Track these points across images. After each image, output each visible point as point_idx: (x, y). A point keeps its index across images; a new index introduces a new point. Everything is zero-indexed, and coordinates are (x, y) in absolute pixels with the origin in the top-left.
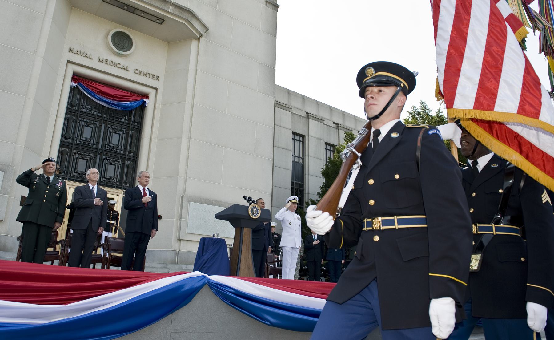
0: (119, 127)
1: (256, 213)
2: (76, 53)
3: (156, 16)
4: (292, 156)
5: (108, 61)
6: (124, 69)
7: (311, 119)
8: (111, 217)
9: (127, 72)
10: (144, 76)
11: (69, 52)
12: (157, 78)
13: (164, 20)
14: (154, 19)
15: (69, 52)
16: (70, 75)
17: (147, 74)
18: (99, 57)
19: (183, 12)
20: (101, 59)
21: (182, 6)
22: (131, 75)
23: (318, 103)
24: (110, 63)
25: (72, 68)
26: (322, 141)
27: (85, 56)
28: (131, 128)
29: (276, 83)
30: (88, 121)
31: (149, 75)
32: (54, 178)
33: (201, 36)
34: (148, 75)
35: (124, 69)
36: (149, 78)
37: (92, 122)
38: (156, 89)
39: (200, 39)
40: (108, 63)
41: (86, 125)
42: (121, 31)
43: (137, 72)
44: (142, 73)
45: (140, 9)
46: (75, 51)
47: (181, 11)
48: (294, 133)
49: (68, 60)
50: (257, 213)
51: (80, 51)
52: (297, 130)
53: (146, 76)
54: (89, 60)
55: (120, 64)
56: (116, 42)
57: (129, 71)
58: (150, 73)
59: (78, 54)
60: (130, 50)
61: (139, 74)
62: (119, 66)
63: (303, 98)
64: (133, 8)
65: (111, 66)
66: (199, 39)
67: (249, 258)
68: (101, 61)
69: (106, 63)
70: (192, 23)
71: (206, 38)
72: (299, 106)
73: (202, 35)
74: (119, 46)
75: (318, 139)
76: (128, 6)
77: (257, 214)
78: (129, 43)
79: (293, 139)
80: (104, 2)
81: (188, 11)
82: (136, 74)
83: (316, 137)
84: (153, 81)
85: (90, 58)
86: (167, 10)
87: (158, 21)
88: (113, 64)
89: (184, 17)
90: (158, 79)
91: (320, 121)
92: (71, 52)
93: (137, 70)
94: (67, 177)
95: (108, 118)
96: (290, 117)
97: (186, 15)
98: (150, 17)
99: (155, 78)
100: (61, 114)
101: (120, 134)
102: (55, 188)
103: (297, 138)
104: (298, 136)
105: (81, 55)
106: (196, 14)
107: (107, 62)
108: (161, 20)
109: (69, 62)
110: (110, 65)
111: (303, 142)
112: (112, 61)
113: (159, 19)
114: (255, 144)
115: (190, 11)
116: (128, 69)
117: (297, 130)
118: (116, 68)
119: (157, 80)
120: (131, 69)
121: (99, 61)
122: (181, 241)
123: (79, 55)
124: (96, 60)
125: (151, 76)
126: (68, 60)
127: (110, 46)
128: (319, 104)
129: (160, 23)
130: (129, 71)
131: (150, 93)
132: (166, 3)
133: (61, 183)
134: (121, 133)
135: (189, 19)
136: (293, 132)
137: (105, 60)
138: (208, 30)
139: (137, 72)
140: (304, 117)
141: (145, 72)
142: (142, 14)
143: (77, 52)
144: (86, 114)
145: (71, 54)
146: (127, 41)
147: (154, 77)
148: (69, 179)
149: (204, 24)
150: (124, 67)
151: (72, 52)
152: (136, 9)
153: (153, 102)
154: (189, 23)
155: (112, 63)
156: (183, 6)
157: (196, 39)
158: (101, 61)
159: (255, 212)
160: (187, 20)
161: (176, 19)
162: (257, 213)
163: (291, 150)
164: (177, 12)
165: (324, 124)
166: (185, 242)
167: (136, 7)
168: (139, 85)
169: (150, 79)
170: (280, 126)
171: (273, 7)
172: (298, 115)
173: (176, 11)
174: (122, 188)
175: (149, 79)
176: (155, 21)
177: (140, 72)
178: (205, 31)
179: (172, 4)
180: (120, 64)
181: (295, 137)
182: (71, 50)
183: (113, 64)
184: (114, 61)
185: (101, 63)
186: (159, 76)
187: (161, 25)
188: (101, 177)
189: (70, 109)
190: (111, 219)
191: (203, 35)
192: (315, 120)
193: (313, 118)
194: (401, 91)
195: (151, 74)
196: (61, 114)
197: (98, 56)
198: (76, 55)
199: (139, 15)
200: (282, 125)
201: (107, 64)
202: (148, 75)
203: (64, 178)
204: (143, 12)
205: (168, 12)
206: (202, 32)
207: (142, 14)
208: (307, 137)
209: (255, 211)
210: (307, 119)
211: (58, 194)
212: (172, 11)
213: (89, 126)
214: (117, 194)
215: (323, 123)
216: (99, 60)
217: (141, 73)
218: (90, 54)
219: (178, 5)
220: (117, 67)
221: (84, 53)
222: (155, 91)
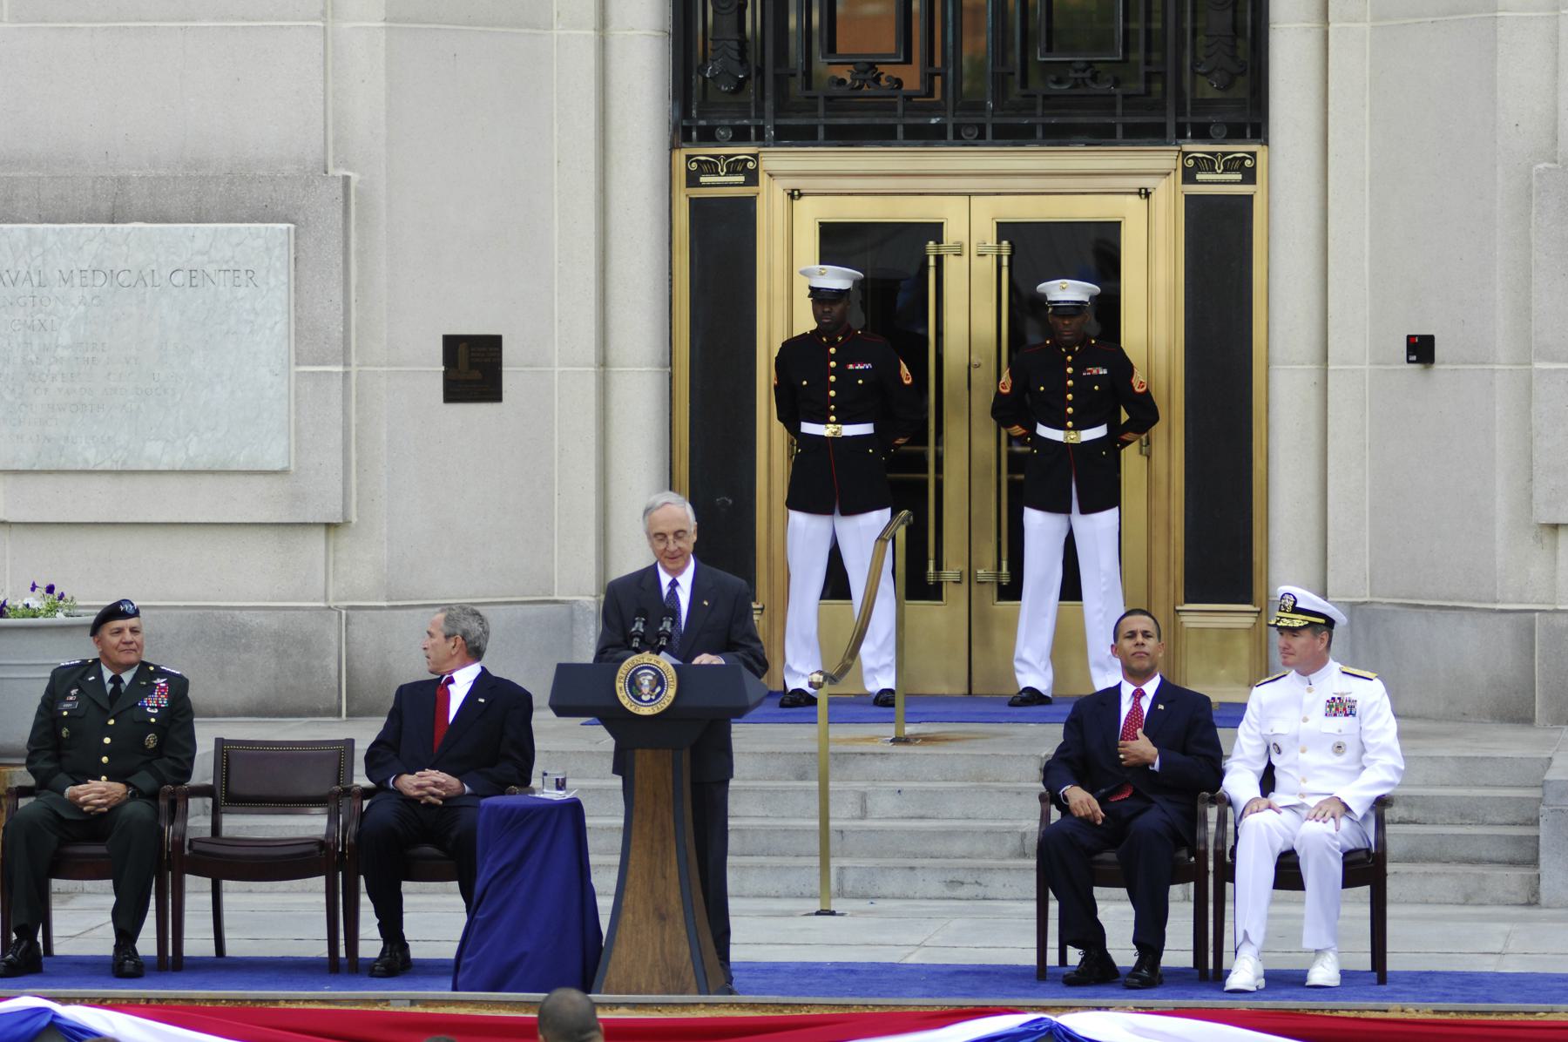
1: (653, 691)
8: (1070, 404)
32: (135, 678)
50: (658, 689)
67: (664, 877)
77: (658, 695)
102: (135, 722)
133: (161, 688)
148: (776, 128)
159: (646, 690)
162: (658, 689)
188: (932, 76)
190: (1070, 417)
203: (748, 128)
209: (646, 683)
211: (151, 740)
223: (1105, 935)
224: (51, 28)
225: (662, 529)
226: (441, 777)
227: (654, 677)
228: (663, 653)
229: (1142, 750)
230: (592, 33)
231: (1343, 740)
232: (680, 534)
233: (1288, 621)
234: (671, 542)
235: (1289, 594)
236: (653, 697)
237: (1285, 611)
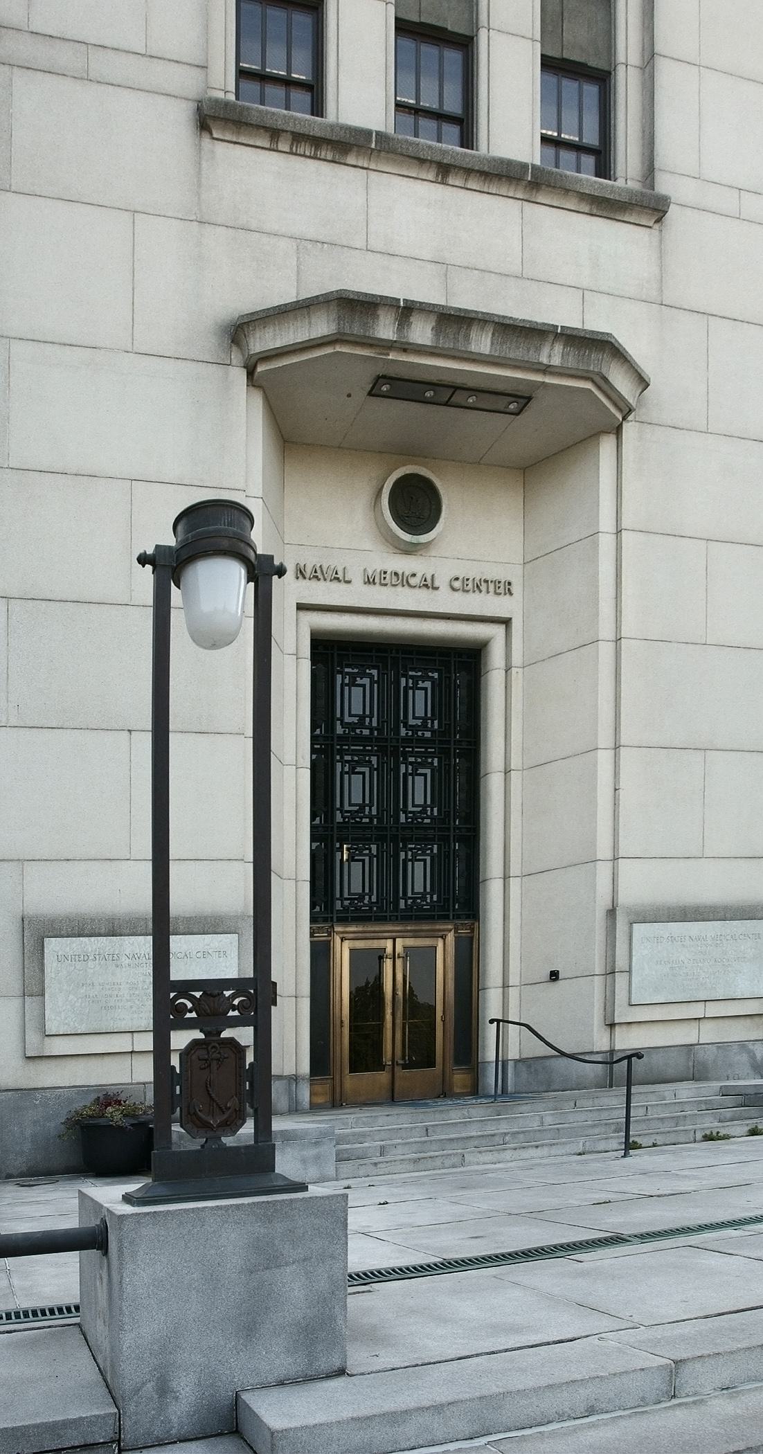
2: (424, 585)
6: (338, 579)
9: (436, 592)
11: (296, 580)
17: (482, 583)
18: (365, 570)
38: (507, 622)
40: (388, 580)
42: (408, 472)
43: (457, 584)
45: (471, 384)
49: (297, 603)
51: (321, 566)
54: (343, 586)
55: (414, 575)
57: (437, 588)
58: (489, 578)
60: (438, 525)
65: (393, 589)
69: (383, 582)
85: (346, 579)
88: (402, 580)
90: (509, 589)
93: (457, 579)
94: (332, 913)
98: (488, 402)
101: (363, 774)
109: (301, 607)
112: (396, 574)
116: (437, 584)
121: (365, 583)
122: (617, 1028)
123: (319, 580)
124: (358, 580)
126: (297, 603)
132: (629, 369)
134: (366, 770)
137: (381, 574)
138: (649, 385)
139: (457, 584)
151: (305, 578)
161: (567, 384)
166: (624, 1028)
169: (491, 597)
174: (451, 917)
176: (502, 409)
177: (383, 576)
183: (402, 580)
194: (598, 148)
196: (303, 758)
197: (362, 569)
198: (314, 583)
199: (462, 407)
204: (513, 399)
213: (418, 772)
214: (440, 934)
216: (366, 580)
218: (344, 568)
222: (498, 631)
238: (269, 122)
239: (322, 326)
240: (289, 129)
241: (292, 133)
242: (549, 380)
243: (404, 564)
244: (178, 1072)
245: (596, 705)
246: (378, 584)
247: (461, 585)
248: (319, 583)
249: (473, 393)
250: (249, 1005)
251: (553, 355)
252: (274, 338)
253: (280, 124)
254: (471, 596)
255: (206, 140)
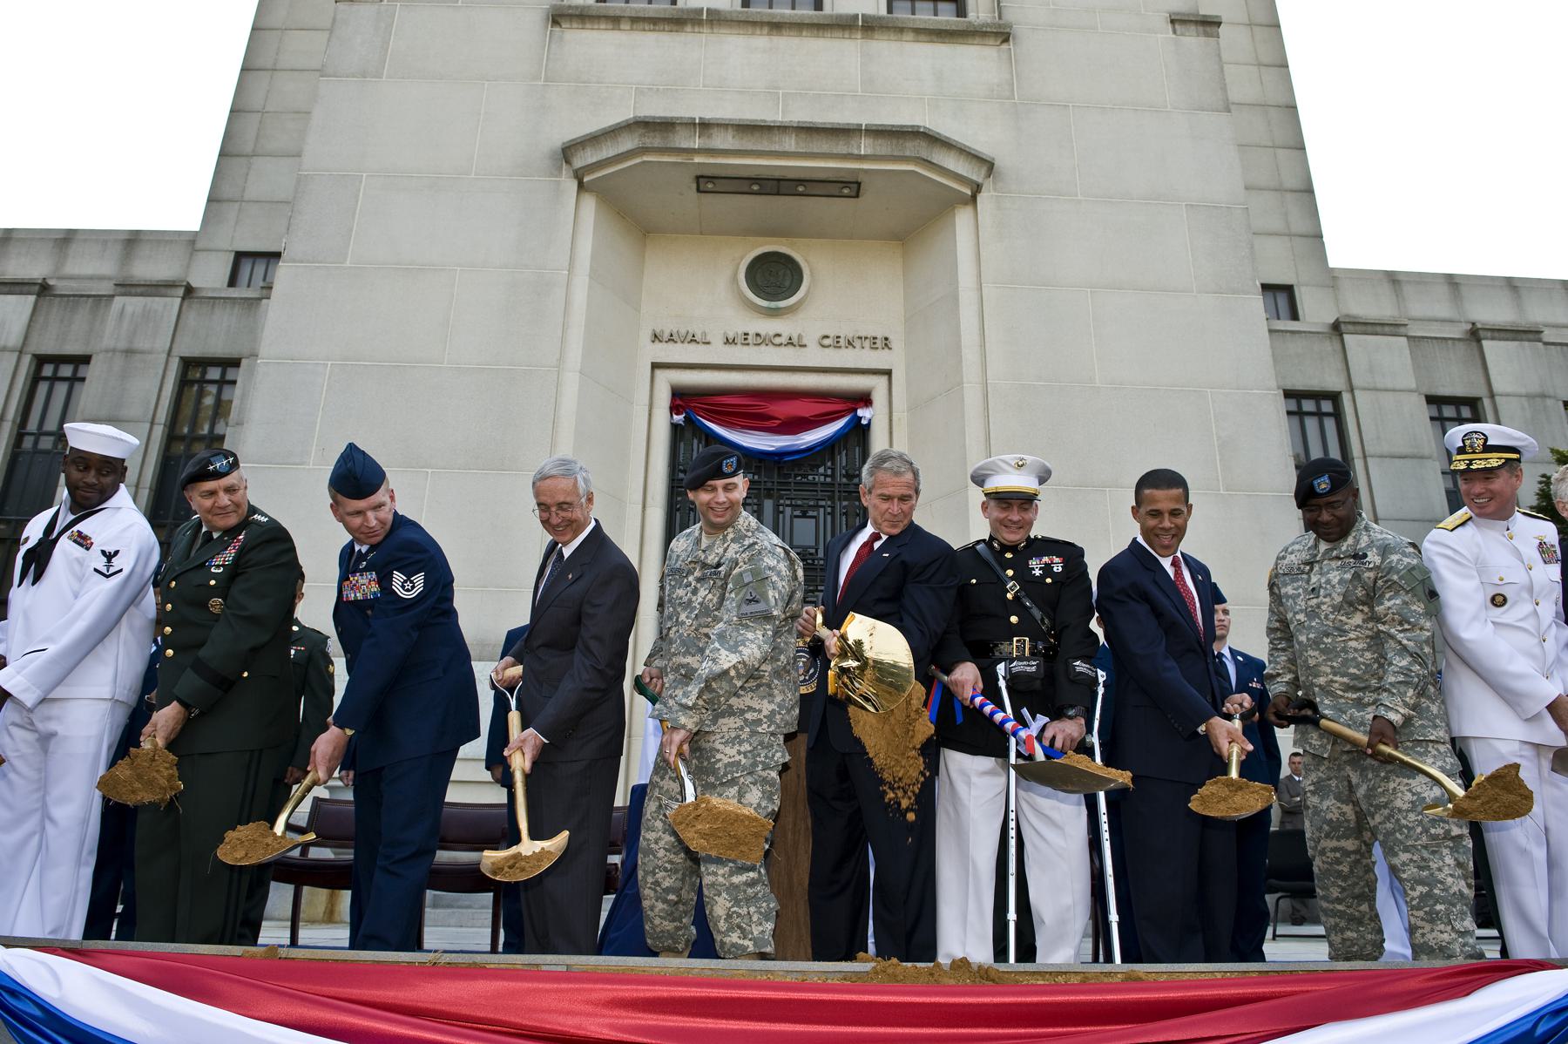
0: (807, 499)
3: (835, 179)
4: (1443, 473)
5: (750, 337)
6: (792, 344)
7: (1486, 339)
9: (803, 349)
10: (847, 347)
12: (884, 342)
13: (859, 184)
14: (833, 189)
15: (653, 342)
16: (664, 398)
19: (901, 142)
20: (731, 337)
21: (893, 126)
22: (814, 356)
23: (1513, 286)
24: (753, 340)
25: (666, 379)
26: (1549, 402)
27: (788, 343)
28: (837, 494)
29: (1332, 264)
30: (799, 502)
31: (859, 341)
33: (977, 188)
34: (857, 343)
35: (792, 344)
36: (863, 348)
37: (812, 503)
38: (888, 373)
39: (978, 198)
40: (750, 341)
41: (797, 513)
42: (766, 251)
44: (841, 340)
46: (666, 336)
47: (894, 141)
48: (1432, 400)
49: (652, 363)
52: (1443, 386)
53: (855, 347)
54: (701, 347)
55: (778, 335)
56: (760, 284)
57: (805, 346)
58: (863, 334)
59: (673, 340)
61: (835, 347)
62: (777, 341)
63: (1453, 283)
64: (771, 182)
65: (756, 348)
66: (974, 198)
68: (731, 341)
70: (935, 161)
71: (995, 190)
72: (1443, 309)
73: (978, 186)
74: (768, 290)
75: (1529, 396)
76: (757, 181)
78: (792, 275)
79: (1432, 419)
80: (703, 194)
81: (912, 132)
82: (826, 350)
83: (1523, 391)
84: (874, 353)
86: (856, 152)
87: (846, 191)
88: (761, 340)
89: (908, 153)
90: (886, 345)
91: (1524, 336)
92: (657, 341)
93: (827, 337)
95: (776, 480)
96: (1407, 352)
97: (912, 147)
99: (879, 344)
100: (653, 499)
103: (1308, 406)
104: (1435, 406)
105: (682, 342)
106: (765, 121)
107: (745, 339)
108: (850, 187)
109: (655, 366)
110: (755, 345)
111: (1338, 415)
112: (758, 335)
113: (846, 184)
114: (1218, 458)
115: (918, 132)
116: (804, 341)
117: (1443, 386)
118: (771, 348)
119: (886, 350)
120: (811, 338)
121: (725, 344)
123: (676, 342)
124: (718, 342)
125: (867, 344)
127: (745, 296)
128: (1519, 285)
129: (854, 194)
130: (805, 346)
131: (873, 388)
135: (924, 155)
136: (1284, 390)
138: (993, 164)
139: (826, 342)
140: (1459, 339)
141: (850, 337)
142: (801, 189)
143: (671, 335)
144: (819, 488)
145: (658, 345)
146: (789, 272)
147: (874, 343)
149: (973, 152)
150: (790, 339)
151: (661, 341)
152: (779, 180)
153: (886, 410)
154: (926, 163)
155: (758, 338)
156: (898, 126)
157: (966, 204)
158: (731, 341)
160: (918, 158)
163: (1435, 455)
164: (883, 147)
165: (1546, 344)
167: (777, 174)
168: (839, 375)
170: (1376, 389)
171: (1201, 29)
172: (1436, 338)
173: (880, 145)
175: (863, 351)
178: (984, 170)
179: (863, 132)
180: (778, 335)
181: (1440, 411)
182: (656, 337)
183: (761, 340)
184: (763, 333)
185: (733, 345)
186: (891, 337)
187: (860, 199)
189: (845, 485)
191: (982, 184)
192: (1507, 340)
193: (1496, 334)
195: (866, 338)
196: (653, 499)
197: (722, 332)
198: (671, 345)
200: (1379, 385)
201: (748, 344)
202: (857, 343)
205: (860, 158)
206: (974, 178)
207: (801, 189)
208: (1487, 402)
210: (1474, 344)
212: (869, 152)
215: (1540, 340)
217: (838, 342)
219: (880, 128)
220: (773, 344)
221: (688, 332)
222: (883, 380)
223: (1147, 473)
224: (321, 263)
225: (549, 501)
226: (1534, 441)
227: (808, 659)
228: (493, 691)
229: (620, 139)
230: (632, 116)
231: (1504, 591)
232: (565, 506)
233: (1483, 462)
234: (554, 514)
235: (1476, 432)
236: (807, 678)
237: (1474, 452)
238: (611, 13)
239: (627, 143)
240: (626, 15)
241: (630, 17)
242: (866, 166)
243: (768, 326)
244: (566, 833)
245: (964, 446)
246: (739, 344)
247: (825, 341)
248: (676, 345)
249: (710, 180)
250: (1410, 820)
251: (865, 146)
252: (592, 156)
253: (618, 13)
254: (844, 352)
255: (557, 29)
